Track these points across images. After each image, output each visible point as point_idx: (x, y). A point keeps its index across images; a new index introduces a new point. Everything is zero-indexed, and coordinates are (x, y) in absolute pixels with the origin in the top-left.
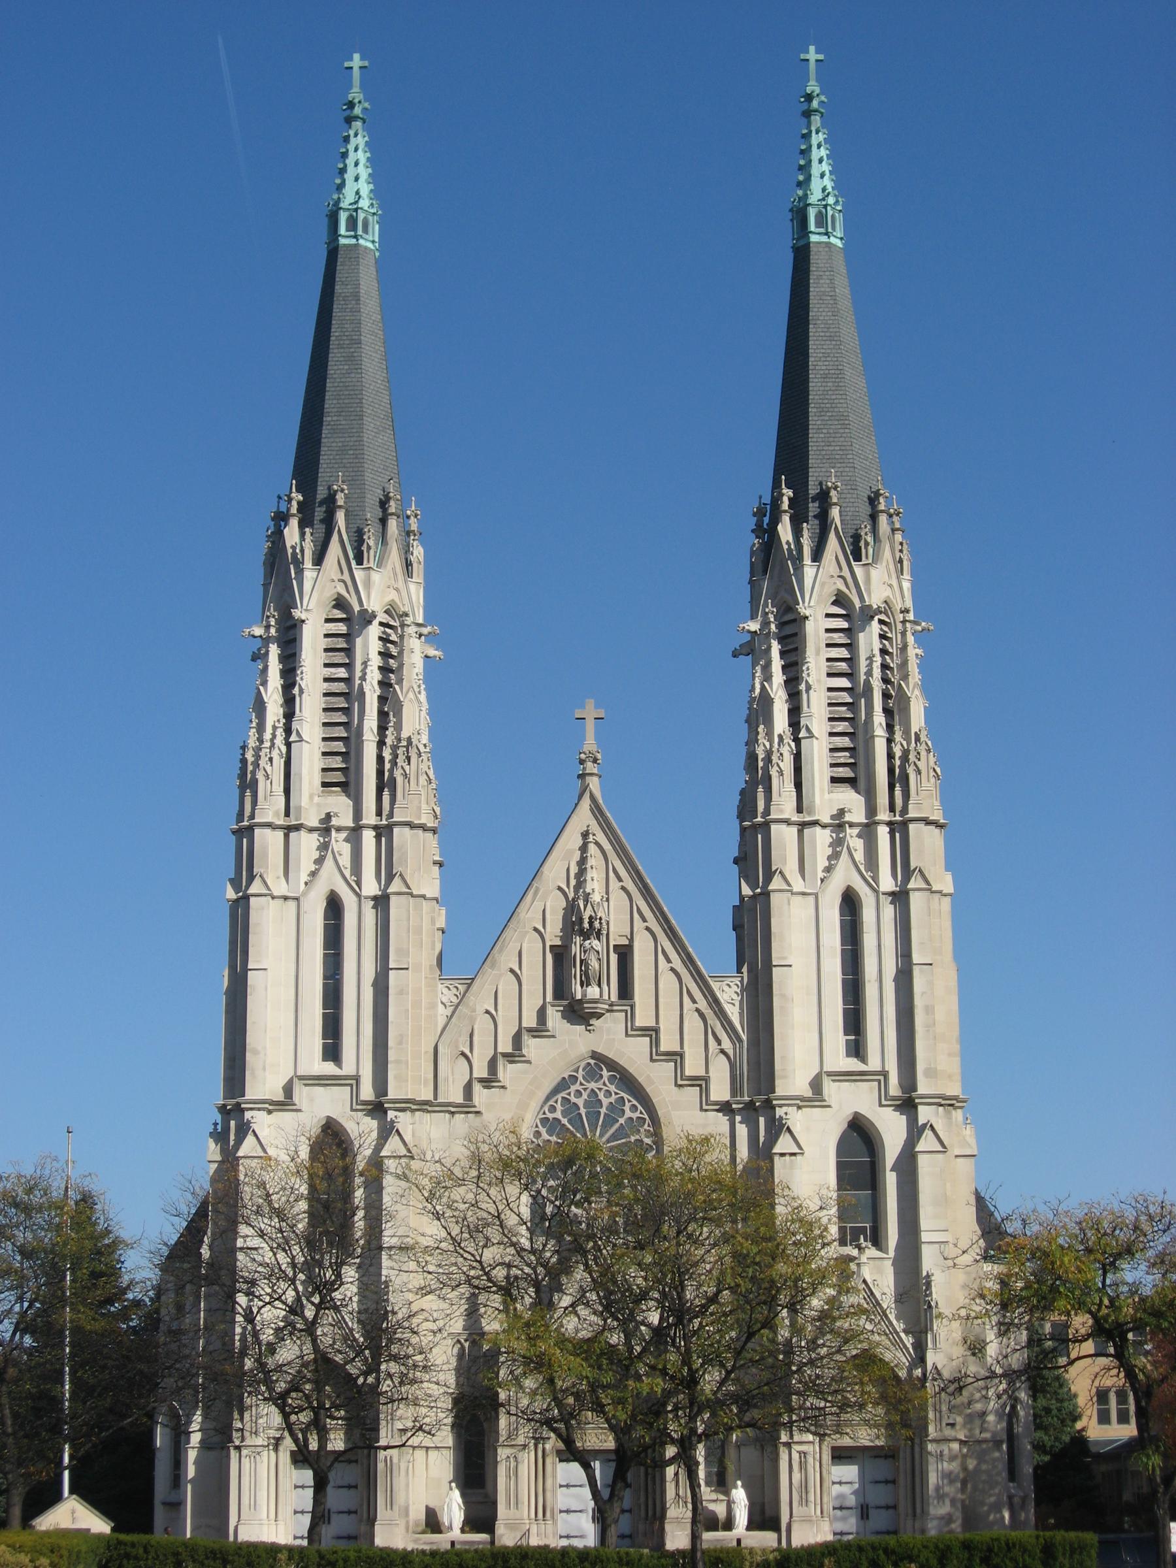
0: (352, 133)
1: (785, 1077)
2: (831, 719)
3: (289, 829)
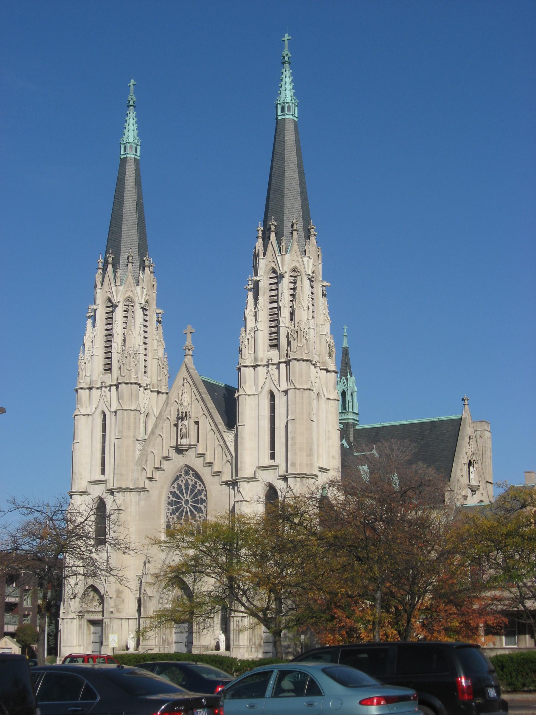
0: (284, 70)
1: (241, 470)
2: (270, 321)
3: (255, 367)
